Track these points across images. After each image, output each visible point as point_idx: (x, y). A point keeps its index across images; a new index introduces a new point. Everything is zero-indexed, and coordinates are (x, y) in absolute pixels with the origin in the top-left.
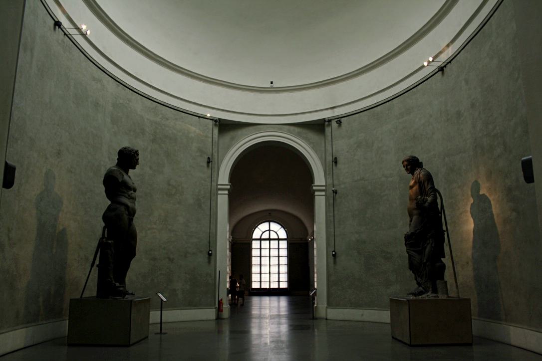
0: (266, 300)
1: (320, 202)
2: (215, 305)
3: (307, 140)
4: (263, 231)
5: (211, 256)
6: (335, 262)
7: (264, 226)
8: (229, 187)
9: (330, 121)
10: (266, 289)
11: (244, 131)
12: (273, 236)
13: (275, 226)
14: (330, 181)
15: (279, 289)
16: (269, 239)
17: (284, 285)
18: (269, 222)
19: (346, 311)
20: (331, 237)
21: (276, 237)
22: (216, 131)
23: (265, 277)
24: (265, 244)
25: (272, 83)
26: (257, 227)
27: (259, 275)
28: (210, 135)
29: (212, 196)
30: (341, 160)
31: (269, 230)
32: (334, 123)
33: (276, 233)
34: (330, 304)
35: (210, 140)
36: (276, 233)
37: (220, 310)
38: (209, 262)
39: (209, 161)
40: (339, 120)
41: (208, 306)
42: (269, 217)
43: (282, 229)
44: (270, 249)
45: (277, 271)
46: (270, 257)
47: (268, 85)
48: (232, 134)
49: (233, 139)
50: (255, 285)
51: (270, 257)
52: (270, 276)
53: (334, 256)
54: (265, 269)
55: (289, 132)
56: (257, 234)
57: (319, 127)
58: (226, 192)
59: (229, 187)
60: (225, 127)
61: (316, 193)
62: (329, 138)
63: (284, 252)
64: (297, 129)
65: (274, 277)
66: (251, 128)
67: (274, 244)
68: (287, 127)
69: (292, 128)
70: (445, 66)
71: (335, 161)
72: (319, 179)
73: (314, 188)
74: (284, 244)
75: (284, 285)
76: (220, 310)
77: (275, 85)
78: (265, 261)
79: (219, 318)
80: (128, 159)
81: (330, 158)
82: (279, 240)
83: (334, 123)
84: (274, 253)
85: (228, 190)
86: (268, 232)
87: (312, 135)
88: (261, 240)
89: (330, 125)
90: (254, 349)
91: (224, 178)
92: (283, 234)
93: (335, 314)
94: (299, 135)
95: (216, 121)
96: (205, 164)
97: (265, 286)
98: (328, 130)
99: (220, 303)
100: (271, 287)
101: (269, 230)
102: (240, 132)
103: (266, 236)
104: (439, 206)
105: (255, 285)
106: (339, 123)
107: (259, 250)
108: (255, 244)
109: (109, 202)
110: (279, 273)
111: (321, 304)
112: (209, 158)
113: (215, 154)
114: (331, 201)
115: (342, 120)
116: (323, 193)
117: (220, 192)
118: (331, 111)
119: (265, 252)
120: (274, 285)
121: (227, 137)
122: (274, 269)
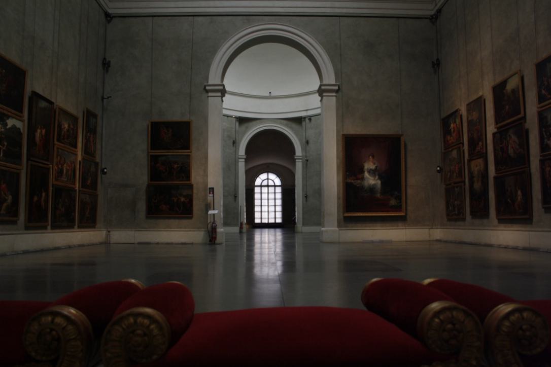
0: (266, 231)
1: (299, 165)
2: (238, 225)
3: (291, 128)
4: (263, 179)
5: (236, 197)
6: (306, 201)
7: (263, 176)
8: (245, 157)
9: (305, 118)
10: (265, 223)
11: (254, 123)
12: (271, 183)
13: (272, 176)
14: (304, 154)
15: (275, 223)
16: (268, 186)
17: (279, 221)
18: (268, 172)
19: (312, 227)
20: (305, 186)
21: (273, 184)
22: (237, 124)
23: (265, 215)
24: (265, 190)
25: (270, 93)
26: (258, 176)
27: (260, 213)
28: (234, 127)
29: (236, 163)
30: (311, 142)
31: (268, 179)
32: (307, 120)
33: (273, 181)
34: (304, 224)
35: (234, 130)
36: (273, 181)
37: (241, 228)
38: (235, 200)
39: (234, 143)
40: (310, 118)
41: (235, 225)
42: (267, 169)
43: (278, 178)
44: (268, 193)
45: (274, 204)
46: (268, 199)
47: (268, 94)
48: (246, 125)
49: (247, 128)
50: (257, 221)
51: (268, 199)
52: (268, 214)
53: (306, 197)
54: (265, 209)
55: (281, 124)
56: (258, 182)
57: (298, 121)
58: (244, 160)
59: (245, 157)
60: (242, 121)
61: (297, 161)
62: (304, 129)
63: (279, 196)
64: (285, 122)
65: (272, 215)
66: (258, 121)
67: (271, 189)
68: (279, 121)
69: (283, 121)
70: (442, 7)
71: (307, 142)
72: (299, 152)
73: (296, 157)
74: (279, 190)
75: (279, 221)
76: (241, 228)
77: (273, 94)
78: (265, 202)
79: (241, 232)
80: (110, 97)
81: (304, 141)
82: (275, 186)
83: (307, 120)
84: (272, 196)
85: (245, 159)
86: (267, 180)
87: (294, 125)
88: (261, 186)
89: (305, 120)
90: (267, 232)
91: (242, 151)
92: (278, 182)
93: (307, 229)
94: (286, 125)
95: (237, 118)
96: (232, 144)
97: (265, 221)
98: (304, 123)
99: (241, 224)
100: (270, 222)
101: (268, 179)
102: (251, 124)
103: (265, 183)
104: (159, 230)
105: (257, 221)
106: (310, 120)
107: (260, 194)
108: (257, 190)
109: (7, 121)
110: (275, 212)
111: (299, 226)
112: (234, 141)
113: (237, 138)
114: (305, 166)
115: (312, 118)
116: (301, 160)
117: (240, 160)
118: (305, 112)
119: (265, 196)
120: (272, 221)
121: (243, 127)
122: (272, 209)
